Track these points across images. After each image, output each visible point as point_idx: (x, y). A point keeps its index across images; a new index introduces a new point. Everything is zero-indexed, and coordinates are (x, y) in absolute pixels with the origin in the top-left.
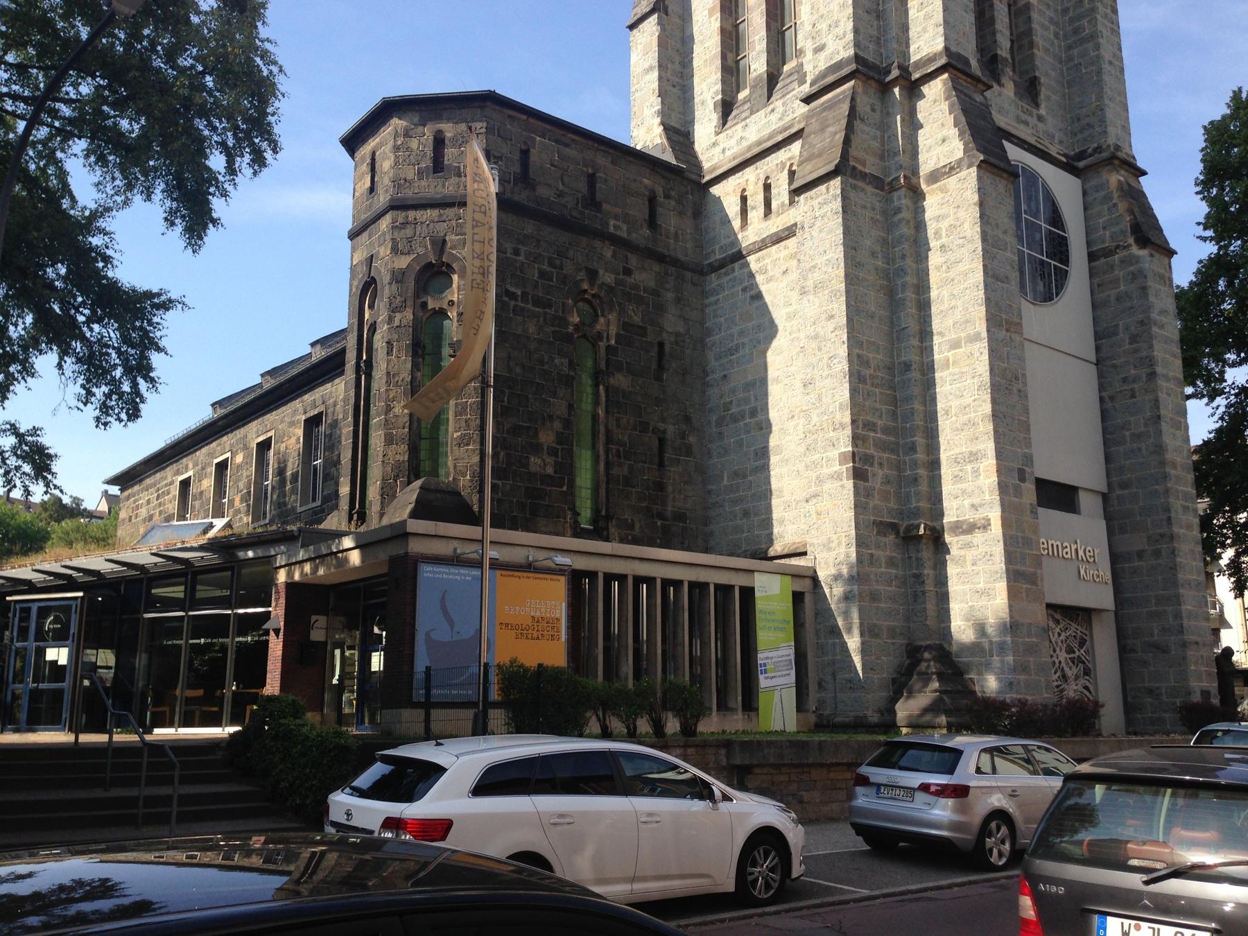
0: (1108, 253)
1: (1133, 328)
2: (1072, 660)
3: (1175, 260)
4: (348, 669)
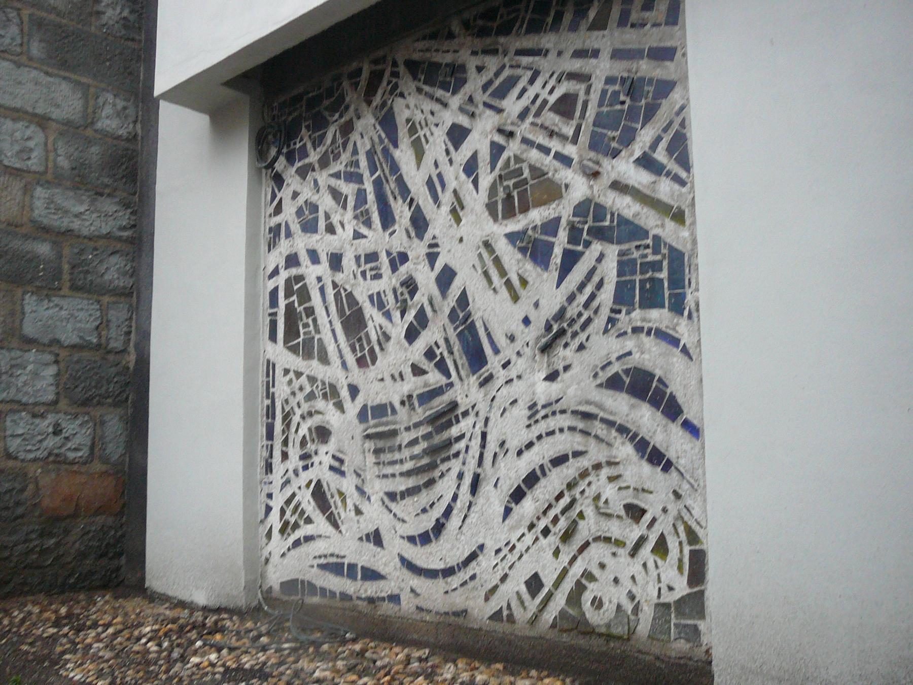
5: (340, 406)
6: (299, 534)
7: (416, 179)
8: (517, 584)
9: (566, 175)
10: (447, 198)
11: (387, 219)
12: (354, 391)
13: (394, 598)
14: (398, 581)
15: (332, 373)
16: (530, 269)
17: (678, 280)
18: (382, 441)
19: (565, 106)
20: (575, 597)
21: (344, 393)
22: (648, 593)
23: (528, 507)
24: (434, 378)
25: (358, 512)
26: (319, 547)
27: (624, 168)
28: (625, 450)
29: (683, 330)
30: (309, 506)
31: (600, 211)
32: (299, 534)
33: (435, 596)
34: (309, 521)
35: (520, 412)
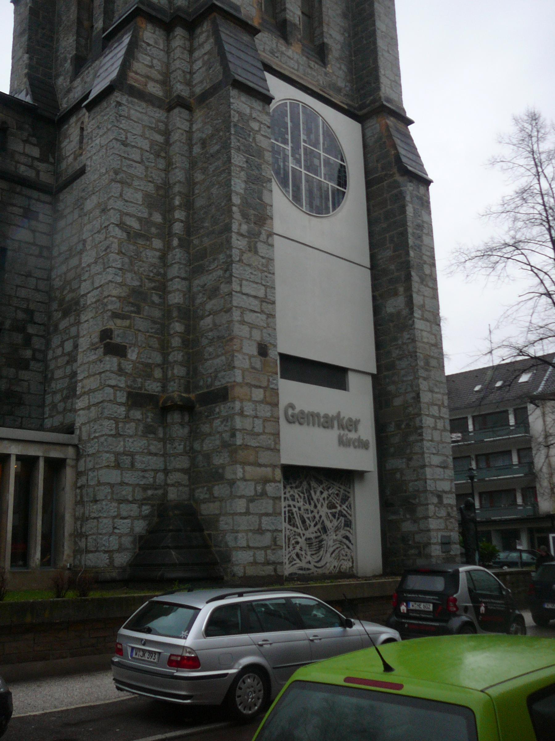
0: (381, 180)
1: (395, 239)
2: (334, 515)
3: (431, 187)
4: (147, 655)
5: (301, 538)
6: (293, 563)
7: (315, 498)
8: (332, 567)
9: (338, 505)
10: (320, 503)
11: (310, 504)
12: (304, 535)
13: (313, 573)
14: (314, 570)
15: (299, 531)
16: (333, 518)
17: (351, 524)
18: (310, 545)
19: (337, 495)
20: (340, 569)
21: (302, 535)
22: (348, 566)
23: (333, 555)
24: (319, 534)
25: (305, 558)
26: (298, 565)
27: (344, 507)
28: (345, 547)
29: (351, 531)
30: (295, 557)
31: (342, 512)
32: (293, 563)
33: (320, 571)
34: (295, 560)
35: (332, 541)
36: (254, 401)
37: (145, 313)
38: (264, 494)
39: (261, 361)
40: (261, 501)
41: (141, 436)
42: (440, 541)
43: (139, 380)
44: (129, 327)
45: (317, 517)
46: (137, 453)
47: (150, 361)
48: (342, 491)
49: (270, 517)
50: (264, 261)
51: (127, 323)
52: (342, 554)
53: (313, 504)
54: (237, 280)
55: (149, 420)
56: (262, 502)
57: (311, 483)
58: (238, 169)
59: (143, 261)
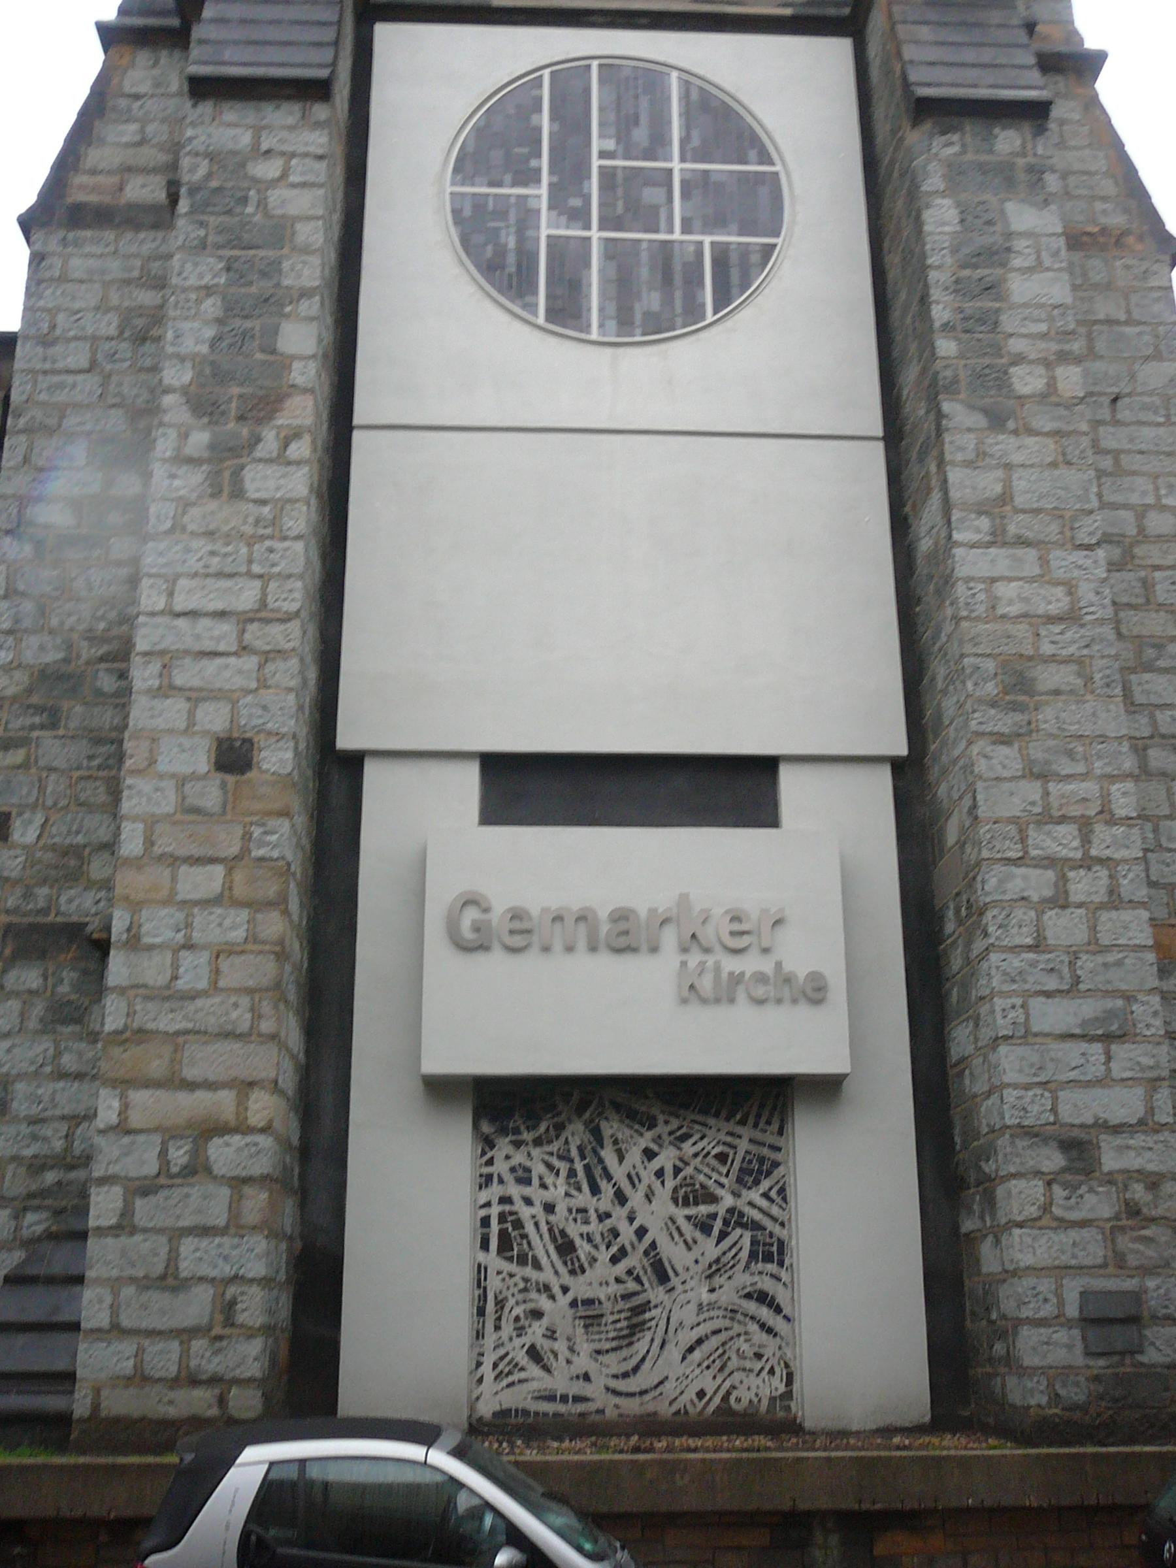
5: (552, 1297)
7: (619, 1173)
8: (691, 1394)
11: (595, 1190)
12: (565, 1290)
13: (601, 1412)
15: (547, 1276)
16: (698, 1235)
19: (722, 1158)
20: (726, 1398)
21: (556, 1290)
22: (766, 1393)
23: (697, 1355)
25: (568, 1362)
26: (534, 1385)
27: (755, 1195)
28: (753, 1327)
30: (522, 1358)
33: (632, 1407)
35: (693, 1307)
36: (184, 902)
37: (72, 725)
38: (197, 1168)
39: (223, 785)
40: (186, 1190)
41: (36, 1032)
42: (1072, 1311)
43: (43, 892)
44: (25, 766)
45: (627, 1233)
46: (20, 1077)
47: (80, 839)
48: (743, 1145)
49: (217, 1240)
50: (266, 510)
51: (18, 756)
52: (741, 1356)
53: (607, 1190)
54: (160, 581)
55: (64, 989)
56: (187, 1196)
57: (604, 1125)
58: (193, 296)
59: (79, 600)
